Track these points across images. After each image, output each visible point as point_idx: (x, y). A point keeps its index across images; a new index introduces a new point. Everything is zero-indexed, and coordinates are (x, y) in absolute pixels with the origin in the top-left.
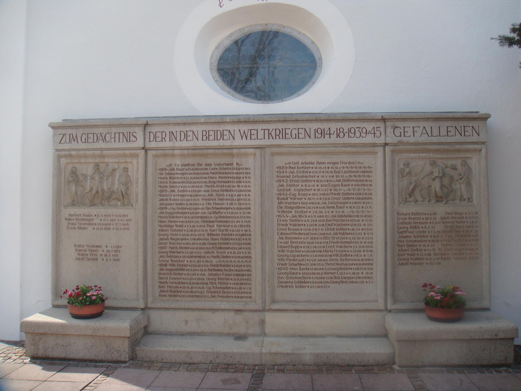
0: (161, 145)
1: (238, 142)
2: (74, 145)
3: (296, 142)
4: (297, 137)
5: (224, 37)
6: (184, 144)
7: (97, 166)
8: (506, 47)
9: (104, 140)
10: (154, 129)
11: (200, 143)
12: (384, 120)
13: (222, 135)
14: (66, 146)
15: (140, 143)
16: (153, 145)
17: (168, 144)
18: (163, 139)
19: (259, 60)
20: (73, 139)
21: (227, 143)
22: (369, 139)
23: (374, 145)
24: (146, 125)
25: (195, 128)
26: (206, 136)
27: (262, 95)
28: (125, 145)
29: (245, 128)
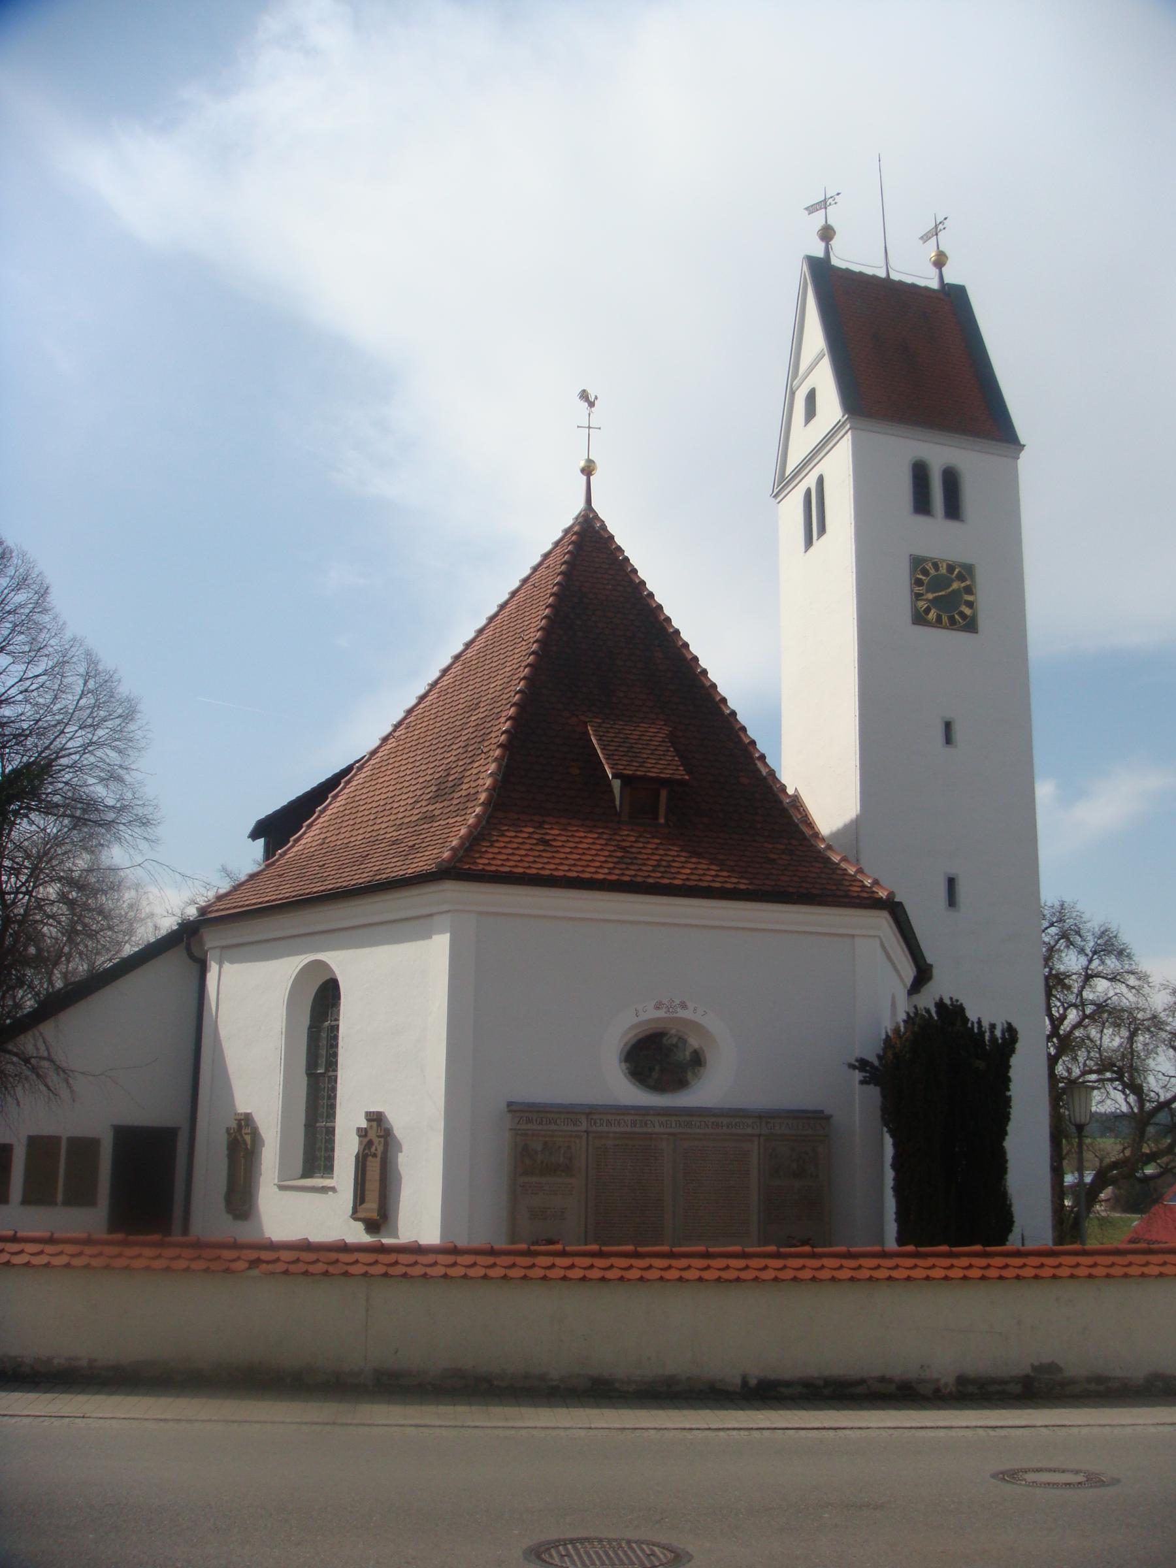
0: (599, 1129)
1: (658, 1129)
2: (529, 1126)
3: (698, 1131)
4: (541, 1123)
5: (631, 1037)
6: (617, 1129)
7: (546, 1143)
8: (851, 1071)
9: (555, 1123)
10: (594, 1117)
11: (629, 1129)
12: (760, 1117)
13: (646, 1124)
14: (524, 1127)
15: (584, 1127)
16: (594, 1128)
17: (605, 1129)
18: (601, 1125)
19: (658, 1057)
20: (529, 1121)
21: (650, 1130)
22: (750, 1131)
23: (753, 1135)
24: (588, 1114)
25: (626, 1118)
26: (634, 1124)
27: (659, 1087)
28: (571, 1128)
29: (664, 1119)
